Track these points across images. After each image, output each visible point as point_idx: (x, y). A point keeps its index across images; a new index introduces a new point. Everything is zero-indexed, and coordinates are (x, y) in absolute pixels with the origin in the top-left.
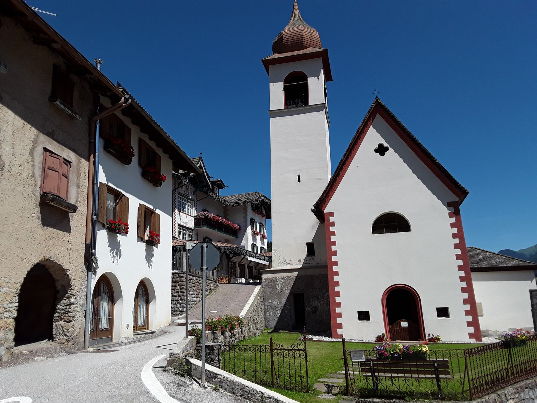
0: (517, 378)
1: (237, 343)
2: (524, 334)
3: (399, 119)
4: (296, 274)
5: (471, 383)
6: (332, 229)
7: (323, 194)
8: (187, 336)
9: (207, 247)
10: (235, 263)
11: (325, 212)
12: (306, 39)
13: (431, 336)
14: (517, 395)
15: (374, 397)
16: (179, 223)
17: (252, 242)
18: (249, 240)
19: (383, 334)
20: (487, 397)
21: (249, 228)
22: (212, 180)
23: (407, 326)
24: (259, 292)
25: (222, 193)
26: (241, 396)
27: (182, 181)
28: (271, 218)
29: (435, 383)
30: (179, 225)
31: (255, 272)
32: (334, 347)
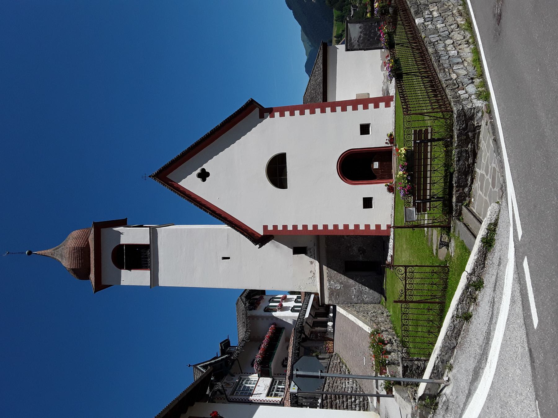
0: (430, 69)
1: (398, 337)
2: (389, 60)
3: (174, 157)
4: (325, 267)
5: (436, 110)
6: (280, 228)
7: (244, 235)
8: (393, 396)
9: (297, 370)
10: (312, 333)
11: (262, 234)
12: (80, 243)
13: (387, 141)
14: (447, 70)
15: (451, 202)
16: (265, 395)
17: (290, 311)
18: (287, 315)
19: (386, 186)
20: (449, 97)
21: (275, 314)
22: (219, 355)
23: (377, 163)
24: (344, 308)
25: (234, 343)
26: (456, 340)
27: (219, 390)
28: (265, 291)
29: (436, 143)
30: (268, 395)
31: (322, 310)
32: (399, 234)
